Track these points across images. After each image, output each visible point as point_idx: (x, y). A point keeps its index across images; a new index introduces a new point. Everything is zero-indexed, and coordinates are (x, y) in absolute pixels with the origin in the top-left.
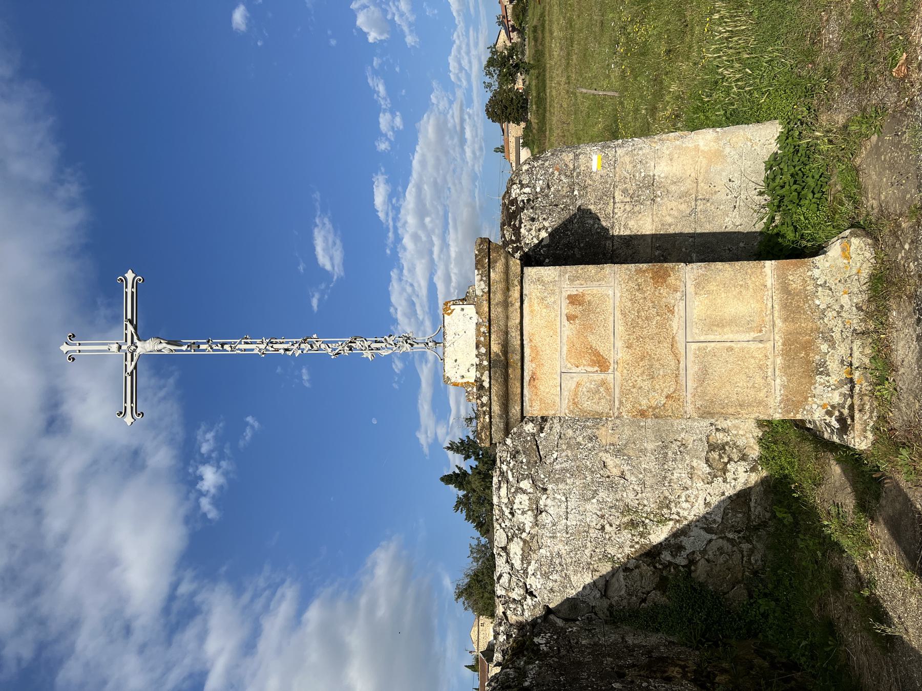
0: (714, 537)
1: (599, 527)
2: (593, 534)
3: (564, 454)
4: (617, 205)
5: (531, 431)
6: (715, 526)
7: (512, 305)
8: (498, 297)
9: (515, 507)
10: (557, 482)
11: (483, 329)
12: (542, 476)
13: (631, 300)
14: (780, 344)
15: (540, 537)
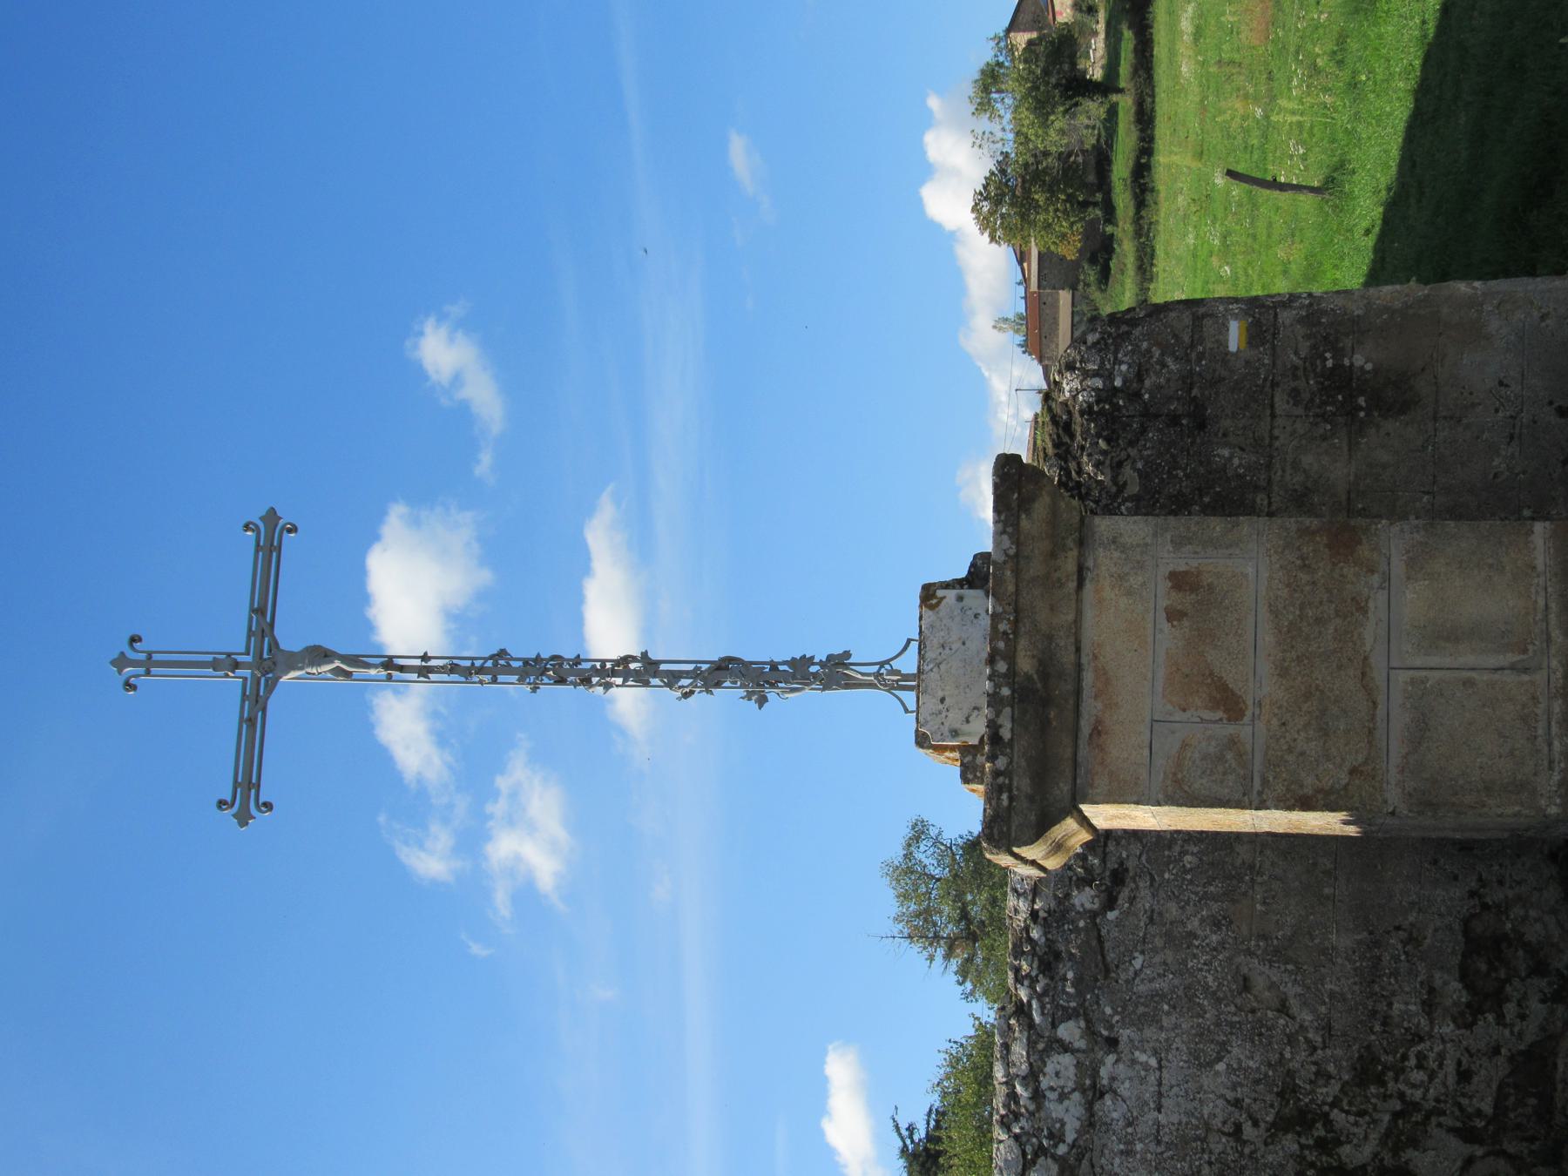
0: (1479, 1152)
1: (1228, 1128)
2: (1219, 1144)
3: (1157, 959)
4: (1279, 422)
5: (1088, 906)
6: (1480, 1124)
7: (1062, 585)
8: (1035, 568)
9: (1045, 1083)
10: (1140, 1022)
11: (1003, 627)
12: (1108, 1011)
13: (1288, 585)
14: (1559, 675)
15: (1096, 1154)
